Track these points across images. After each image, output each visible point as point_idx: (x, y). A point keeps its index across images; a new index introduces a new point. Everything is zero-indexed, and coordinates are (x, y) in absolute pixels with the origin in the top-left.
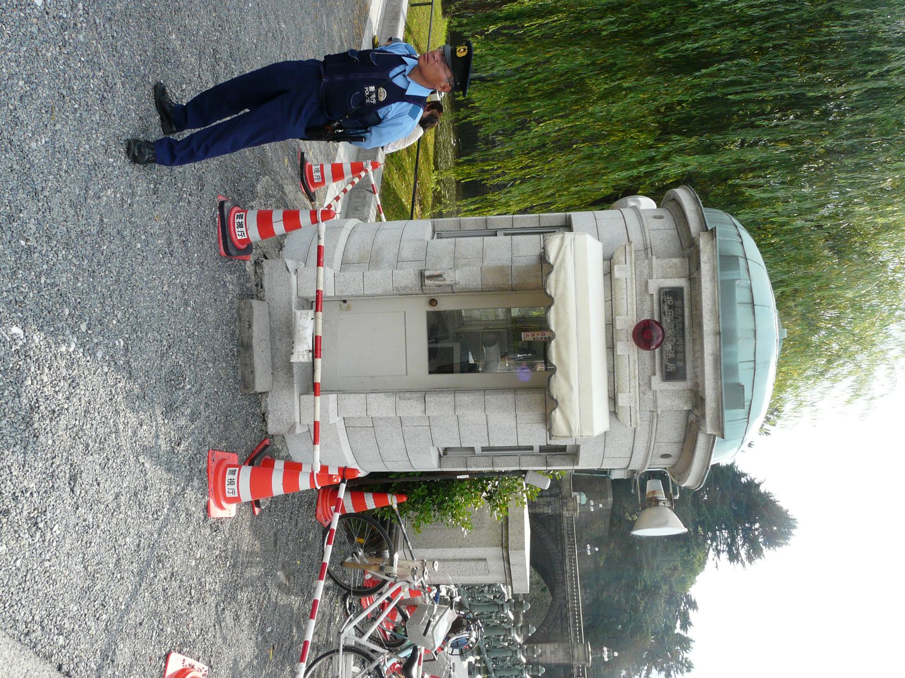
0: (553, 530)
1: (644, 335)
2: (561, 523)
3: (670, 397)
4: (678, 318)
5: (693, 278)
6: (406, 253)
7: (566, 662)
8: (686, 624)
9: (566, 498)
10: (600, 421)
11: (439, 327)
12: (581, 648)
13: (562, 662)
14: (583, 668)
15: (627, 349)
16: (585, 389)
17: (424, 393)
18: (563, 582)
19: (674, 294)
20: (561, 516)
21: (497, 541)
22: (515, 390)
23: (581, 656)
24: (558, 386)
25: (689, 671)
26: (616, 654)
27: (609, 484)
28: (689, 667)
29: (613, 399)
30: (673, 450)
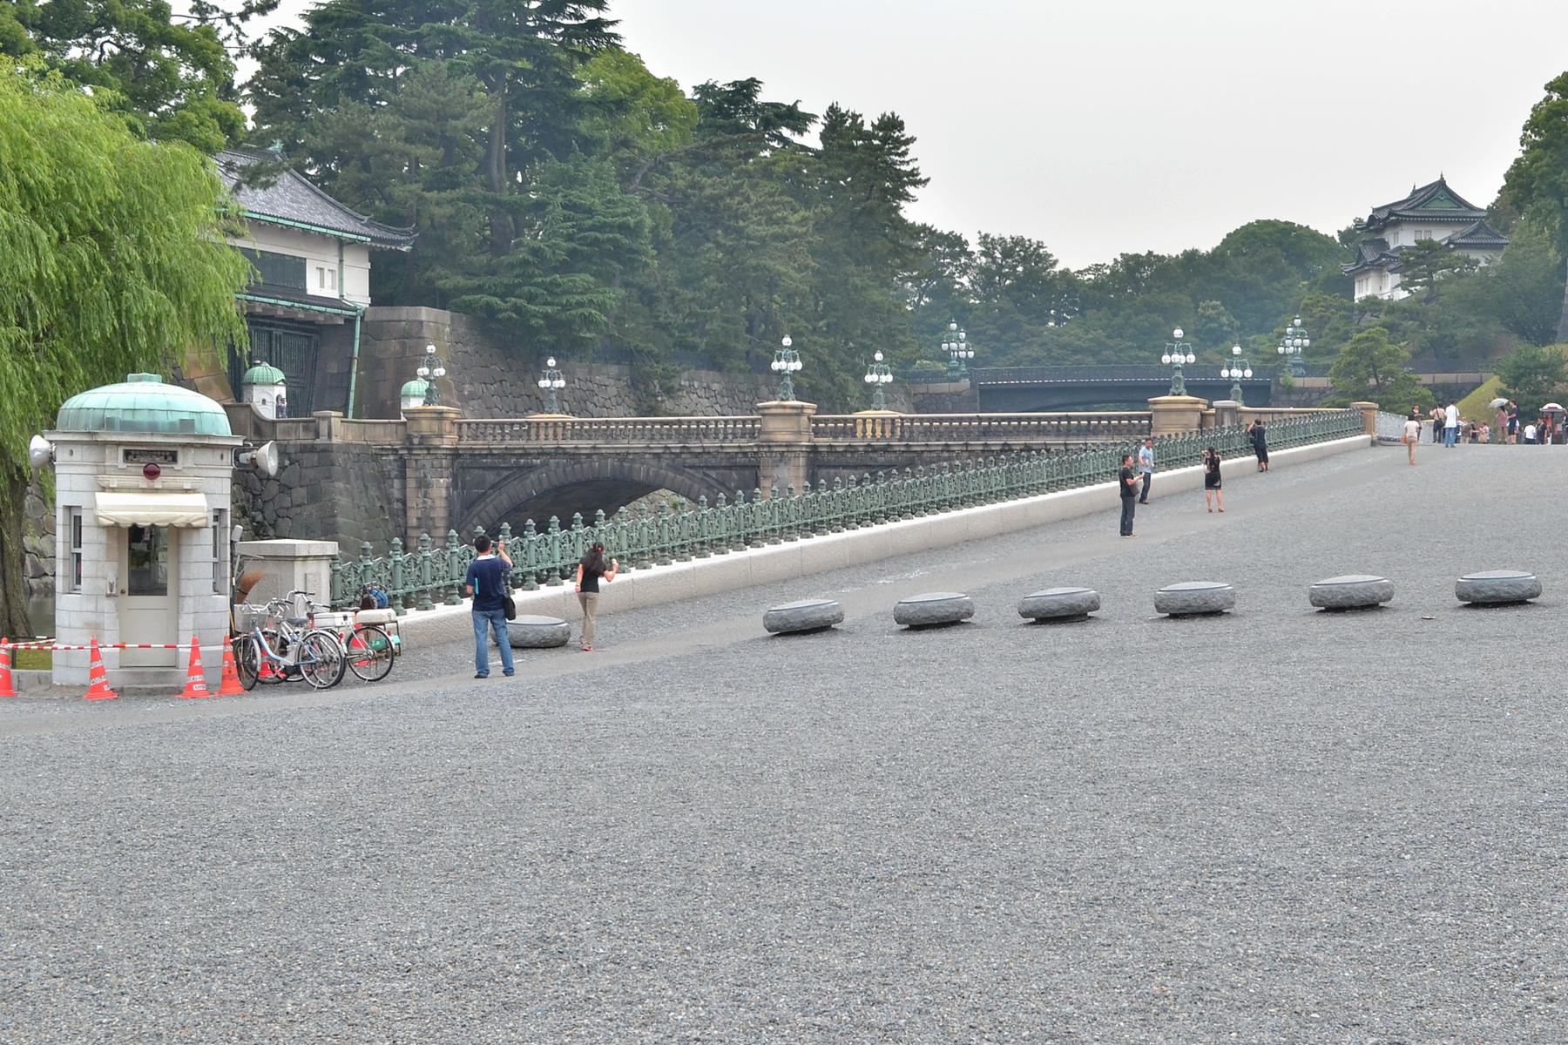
0: (491, 477)
1: (151, 474)
2: (474, 455)
3: (185, 460)
4: (141, 453)
5: (119, 444)
6: (91, 607)
7: (802, 461)
8: (796, 118)
9: (409, 437)
10: (198, 500)
11: (135, 590)
12: (772, 425)
13: (802, 472)
14: (817, 421)
15: (158, 484)
16: (182, 509)
17: (179, 596)
18: (622, 457)
19: (127, 454)
20: (455, 454)
21: (288, 564)
22: (179, 545)
23: (789, 424)
24: (178, 522)
25: (899, 125)
26: (787, 341)
27: (385, 313)
28: (891, 124)
29: (187, 491)
30: (218, 453)
